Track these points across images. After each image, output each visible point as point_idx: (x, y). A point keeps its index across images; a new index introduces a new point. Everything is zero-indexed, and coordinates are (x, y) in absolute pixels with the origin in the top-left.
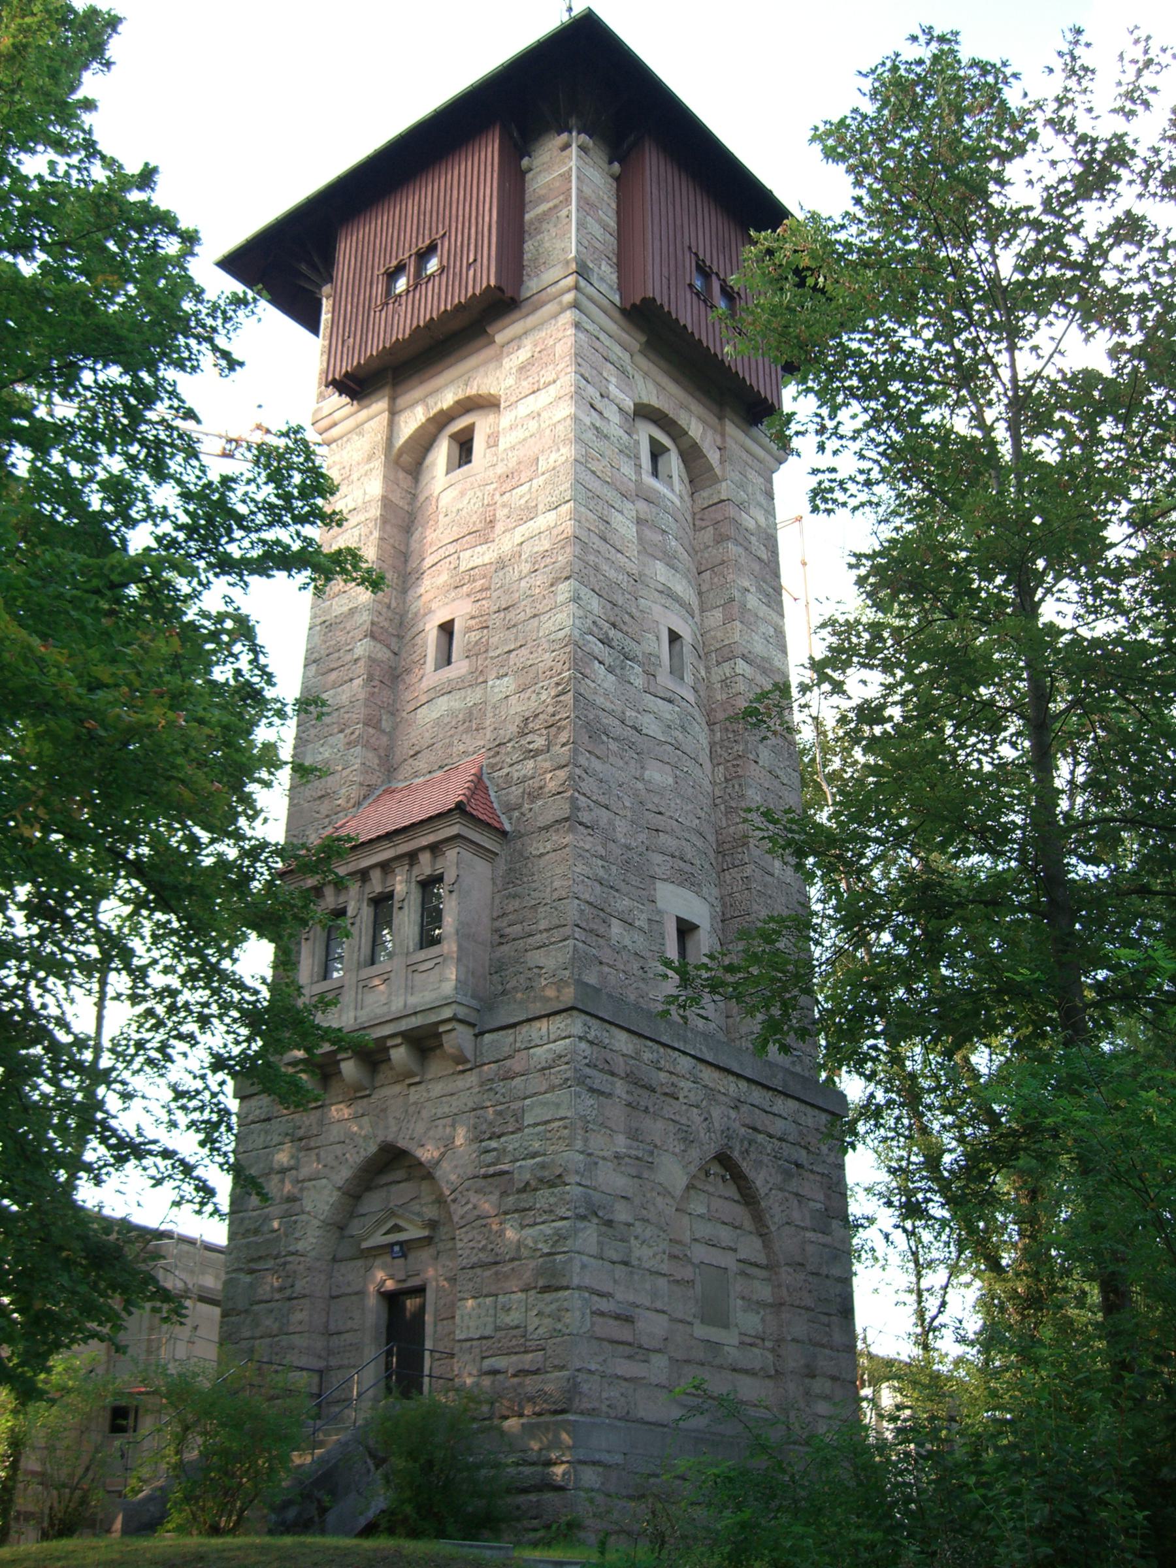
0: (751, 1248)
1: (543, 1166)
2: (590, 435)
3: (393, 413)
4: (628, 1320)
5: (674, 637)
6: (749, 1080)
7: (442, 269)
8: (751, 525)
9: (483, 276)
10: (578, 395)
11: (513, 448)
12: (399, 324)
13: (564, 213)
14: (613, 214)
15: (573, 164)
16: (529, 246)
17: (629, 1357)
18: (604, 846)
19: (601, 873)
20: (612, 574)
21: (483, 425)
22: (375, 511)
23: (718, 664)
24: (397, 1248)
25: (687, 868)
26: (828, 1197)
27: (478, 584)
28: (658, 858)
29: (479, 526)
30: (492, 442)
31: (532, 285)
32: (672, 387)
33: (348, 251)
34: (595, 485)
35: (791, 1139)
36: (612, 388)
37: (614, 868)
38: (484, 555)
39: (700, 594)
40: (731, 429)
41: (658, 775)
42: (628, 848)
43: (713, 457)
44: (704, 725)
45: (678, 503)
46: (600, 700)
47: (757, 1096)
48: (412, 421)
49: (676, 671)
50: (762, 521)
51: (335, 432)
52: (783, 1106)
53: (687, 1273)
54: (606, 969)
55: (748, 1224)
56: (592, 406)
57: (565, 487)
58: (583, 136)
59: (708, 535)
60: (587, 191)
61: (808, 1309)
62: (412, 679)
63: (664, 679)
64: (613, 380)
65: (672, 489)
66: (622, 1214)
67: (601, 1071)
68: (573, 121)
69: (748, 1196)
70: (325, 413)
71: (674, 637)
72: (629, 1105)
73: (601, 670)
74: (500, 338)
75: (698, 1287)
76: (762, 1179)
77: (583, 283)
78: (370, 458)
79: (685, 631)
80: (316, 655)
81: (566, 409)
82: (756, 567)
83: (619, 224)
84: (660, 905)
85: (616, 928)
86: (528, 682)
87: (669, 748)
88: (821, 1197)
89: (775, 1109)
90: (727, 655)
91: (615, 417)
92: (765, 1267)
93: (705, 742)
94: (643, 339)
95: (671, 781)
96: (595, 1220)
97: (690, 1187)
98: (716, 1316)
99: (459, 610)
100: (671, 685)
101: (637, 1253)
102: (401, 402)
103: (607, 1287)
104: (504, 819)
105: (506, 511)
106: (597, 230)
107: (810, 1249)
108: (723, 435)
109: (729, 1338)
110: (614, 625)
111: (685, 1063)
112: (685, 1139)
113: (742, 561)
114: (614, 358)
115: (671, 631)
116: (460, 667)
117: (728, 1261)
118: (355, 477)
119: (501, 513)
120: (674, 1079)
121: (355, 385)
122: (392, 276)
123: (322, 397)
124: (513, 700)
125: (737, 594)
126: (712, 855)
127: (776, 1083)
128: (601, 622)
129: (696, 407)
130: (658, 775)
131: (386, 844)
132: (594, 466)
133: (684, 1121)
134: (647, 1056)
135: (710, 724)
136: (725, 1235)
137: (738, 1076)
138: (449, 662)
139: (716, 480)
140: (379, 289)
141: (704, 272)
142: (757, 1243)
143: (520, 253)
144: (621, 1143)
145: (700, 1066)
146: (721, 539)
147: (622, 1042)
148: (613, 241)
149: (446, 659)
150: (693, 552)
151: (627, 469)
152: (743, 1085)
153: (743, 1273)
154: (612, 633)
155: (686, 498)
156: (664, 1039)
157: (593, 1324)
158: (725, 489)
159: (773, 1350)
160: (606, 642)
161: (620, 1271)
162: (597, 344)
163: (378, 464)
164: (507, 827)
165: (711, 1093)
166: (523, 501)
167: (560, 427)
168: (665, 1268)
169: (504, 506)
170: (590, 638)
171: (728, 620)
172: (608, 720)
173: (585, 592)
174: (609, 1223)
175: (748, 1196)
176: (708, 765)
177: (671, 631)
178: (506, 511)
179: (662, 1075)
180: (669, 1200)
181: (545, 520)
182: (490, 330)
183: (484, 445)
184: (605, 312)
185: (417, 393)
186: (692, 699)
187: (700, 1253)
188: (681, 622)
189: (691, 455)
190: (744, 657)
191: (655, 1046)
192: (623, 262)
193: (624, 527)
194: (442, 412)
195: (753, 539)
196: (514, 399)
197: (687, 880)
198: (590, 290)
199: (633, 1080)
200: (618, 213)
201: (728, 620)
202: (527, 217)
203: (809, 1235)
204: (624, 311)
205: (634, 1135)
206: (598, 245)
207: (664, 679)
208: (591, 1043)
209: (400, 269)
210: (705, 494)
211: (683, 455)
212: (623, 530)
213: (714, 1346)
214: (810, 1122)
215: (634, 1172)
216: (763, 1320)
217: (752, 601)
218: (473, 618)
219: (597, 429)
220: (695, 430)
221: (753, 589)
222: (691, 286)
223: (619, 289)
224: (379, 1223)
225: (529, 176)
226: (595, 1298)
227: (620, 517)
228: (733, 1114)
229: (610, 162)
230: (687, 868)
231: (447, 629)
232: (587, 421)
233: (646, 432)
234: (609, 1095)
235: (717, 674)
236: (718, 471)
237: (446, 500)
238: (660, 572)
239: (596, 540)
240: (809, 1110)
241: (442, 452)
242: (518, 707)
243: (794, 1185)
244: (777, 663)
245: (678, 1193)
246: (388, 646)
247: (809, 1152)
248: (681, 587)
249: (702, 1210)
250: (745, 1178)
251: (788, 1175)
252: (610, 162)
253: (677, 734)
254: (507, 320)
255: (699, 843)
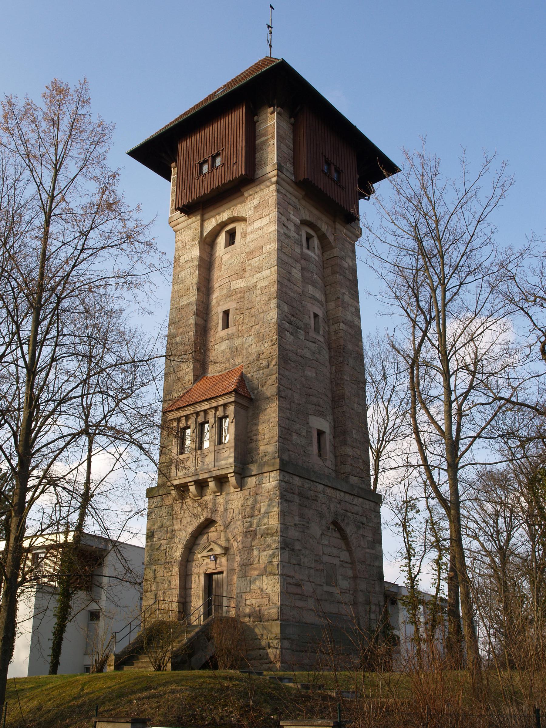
0: (345, 556)
1: (268, 529)
2: (283, 238)
3: (203, 221)
4: (300, 586)
5: (316, 316)
6: (344, 492)
7: (223, 165)
8: (346, 265)
9: (240, 170)
10: (280, 222)
11: (252, 241)
12: (205, 187)
13: (271, 143)
14: (291, 141)
15: (275, 121)
16: (258, 155)
17: (300, 599)
18: (290, 405)
19: (289, 415)
20: (292, 295)
21: (240, 228)
22: (196, 263)
23: (333, 324)
24: (212, 557)
25: (321, 409)
26: (374, 535)
27: (239, 295)
28: (310, 406)
29: (239, 271)
30: (243, 235)
31: (259, 173)
32: (315, 211)
33: (182, 147)
34: (285, 258)
35: (360, 513)
36: (292, 216)
37: (293, 413)
38: (240, 284)
39: (326, 295)
40: (338, 226)
41: (310, 373)
42: (299, 404)
43: (331, 238)
44: (327, 350)
45: (317, 258)
46: (288, 347)
47: (348, 498)
48: (210, 225)
49: (317, 330)
50: (351, 263)
51: (179, 227)
52: (358, 501)
53: (321, 567)
54: (291, 453)
55: (344, 547)
56: (284, 225)
57: (274, 259)
58: (279, 108)
59: (328, 271)
60: (281, 132)
61: (366, 579)
62: (212, 332)
63: (312, 334)
64: (292, 212)
65: (314, 254)
66: (298, 546)
67: (290, 492)
68: (275, 102)
69: (344, 537)
70: (175, 218)
71: (316, 316)
72: (300, 505)
73: (288, 334)
74: (246, 195)
75: (325, 571)
76: (349, 530)
77: (280, 173)
78: (193, 240)
79: (320, 313)
80: (174, 321)
81: (273, 227)
82: (348, 283)
83: (294, 145)
84: (310, 425)
85: (295, 437)
86: (261, 338)
87: (314, 361)
88: (371, 535)
89: (354, 503)
90: (336, 321)
91: (292, 228)
92: (351, 563)
93: (327, 357)
94: (304, 193)
95: (314, 375)
96: (288, 549)
97: (322, 534)
98: (331, 580)
99: (231, 305)
100: (315, 336)
101: (302, 560)
102: (206, 216)
103: (292, 574)
104: (251, 393)
105: (250, 267)
106: (285, 149)
107: (367, 555)
108: (335, 229)
109: (336, 590)
110: (293, 316)
111: (320, 487)
112: (320, 517)
113: (343, 282)
114: (292, 203)
115: (314, 314)
116: (232, 330)
117: (336, 561)
118: (188, 247)
119: (248, 268)
120: (316, 494)
121: (187, 209)
122: (201, 165)
123: (172, 212)
124: (254, 346)
125: (340, 296)
126: (330, 402)
127: (355, 493)
128: (288, 315)
129: (324, 218)
130: (310, 373)
131: (206, 403)
132: (285, 250)
133: (320, 509)
134: (306, 486)
135: (330, 349)
136: (335, 551)
137: (340, 491)
138: (227, 327)
139: (332, 248)
140: (197, 170)
141: (328, 163)
142: (347, 554)
143: (254, 158)
144: (297, 520)
145: (327, 488)
146: (334, 273)
147: (297, 481)
148: (291, 152)
149: (226, 325)
150: (323, 278)
151: (298, 250)
152: (342, 494)
153: (342, 566)
154: (292, 319)
155: (321, 256)
156: (314, 479)
157: (287, 588)
158: (336, 252)
159: (353, 595)
160: (290, 323)
161: (297, 567)
162: (285, 198)
163: (197, 242)
164: (253, 397)
165: (330, 499)
166: (257, 264)
167: (271, 235)
168: (313, 566)
169: (249, 265)
170: (284, 322)
171: (337, 306)
172: (290, 354)
173: (282, 303)
174: (293, 550)
175: (344, 537)
176: (329, 367)
177: (314, 314)
178: (250, 267)
179: (312, 492)
180: (314, 540)
181: (266, 273)
182: (242, 190)
183: (240, 237)
184: (288, 184)
185: (212, 213)
186: (322, 340)
187: (326, 559)
188: (319, 309)
189: (322, 238)
190: (343, 322)
191: (309, 482)
192: (295, 162)
193: (297, 274)
194: (222, 222)
195: (347, 271)
196: (252, 220)
197: (321, 414)
198: (283, 176)
199: (301, 495)
200: (293, 139)
201: (337, 306)
202: (257, 142)
203: (367, 550)
204: (295, 183)
205: (301, 516)
206: (286, 155)
207: (312, 334)
208: (285, 482)
209: (205, 162)
210: (328, 253)
211: (319, 238)
212: (296, 276)
213: (331, 594)
214: (367, 507)
215: (301, 530)
216: (349, 583)
217: (347, 298)
218: (237, 309)
219: (286, 234)
220: (324, 228)
221: (347, 293)
222: (323, 171)
223: (294, 173)
224: (205, 548)
225: (257, 124)
226: (288, 578)
227: (295, 270)
228: (338, 506)
229: (290, 118)
230: (321, 409)
231: (226, 313)
232: (282, 231)
233: (305, 230)
234: (293, 502)
235: (333, 328)
236: (333, 244)
237: (225, 258)
238: (311, 289)
239: (285, 281)
240: (367, 502)
241: (222, 239)
242: (255, 349)
243: (361, 532)
244: (356, 323)
245: (318, 537)
246: (203, 318)
247: (367, 518)
248: (319, 295)
249: (327, 543)
250: (343, 530)
251: (359, 528)
252: (290, 118)
253: (317, 356)
254: (249, 187)
255: (326, 399)
